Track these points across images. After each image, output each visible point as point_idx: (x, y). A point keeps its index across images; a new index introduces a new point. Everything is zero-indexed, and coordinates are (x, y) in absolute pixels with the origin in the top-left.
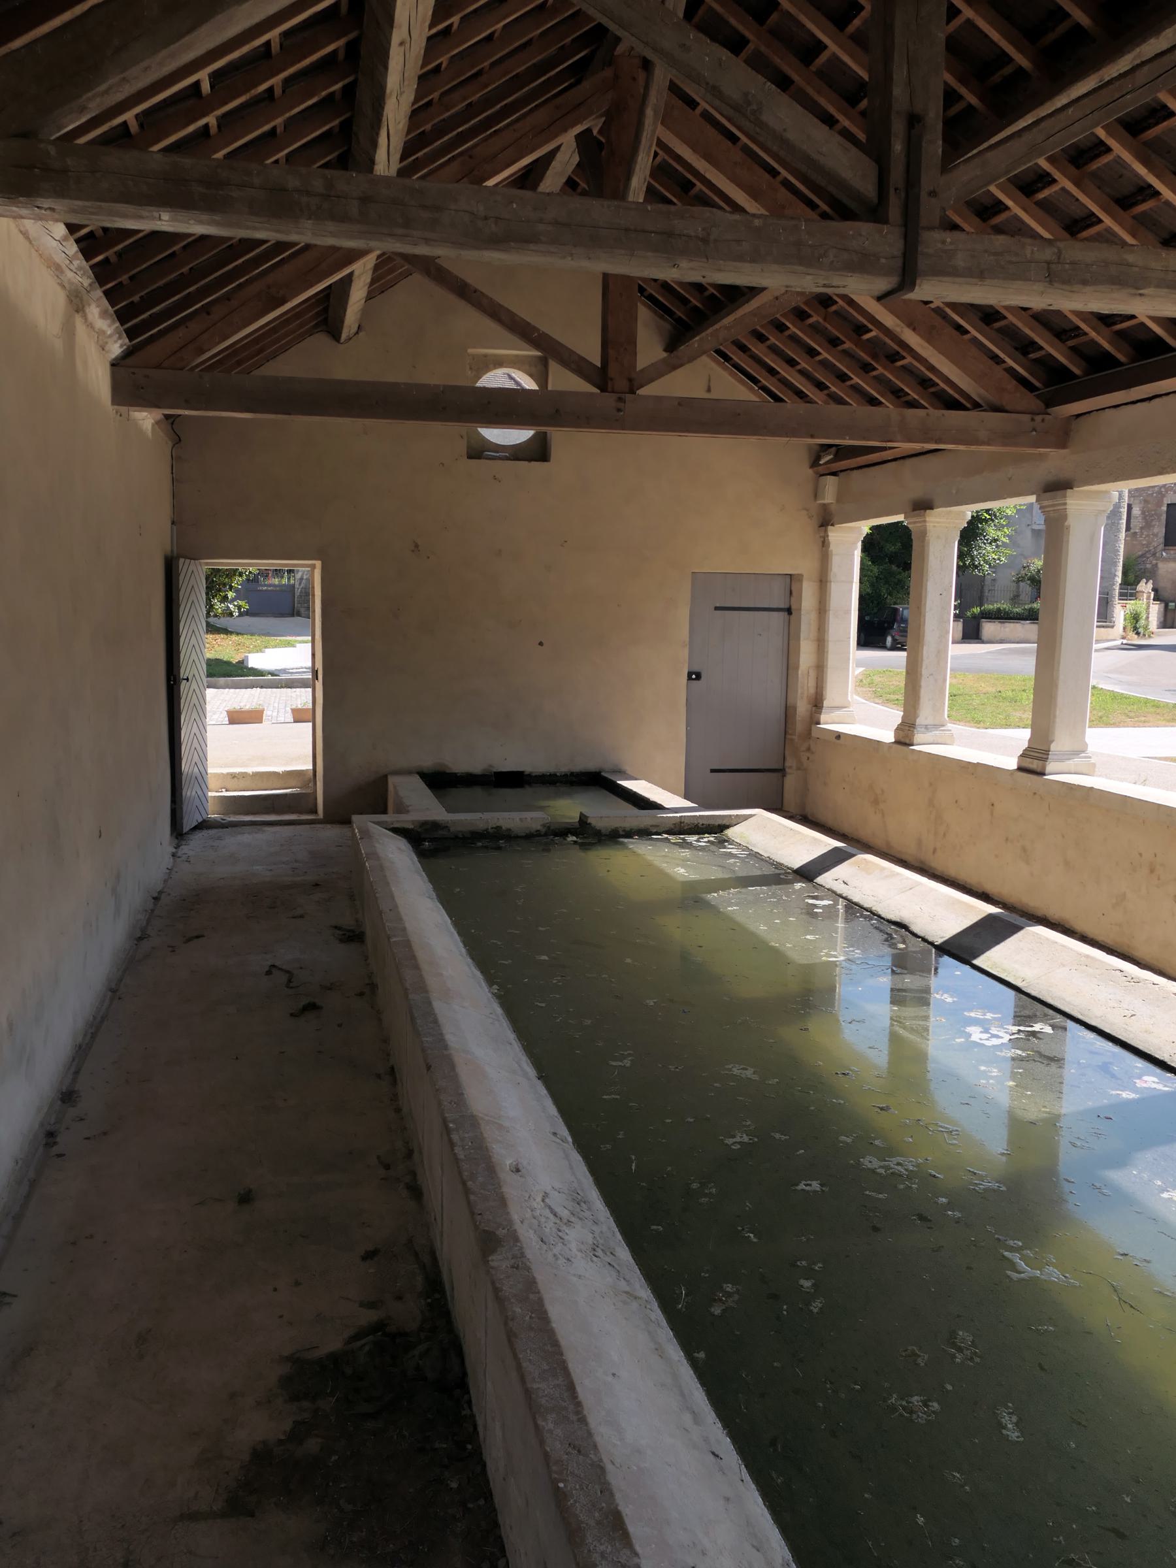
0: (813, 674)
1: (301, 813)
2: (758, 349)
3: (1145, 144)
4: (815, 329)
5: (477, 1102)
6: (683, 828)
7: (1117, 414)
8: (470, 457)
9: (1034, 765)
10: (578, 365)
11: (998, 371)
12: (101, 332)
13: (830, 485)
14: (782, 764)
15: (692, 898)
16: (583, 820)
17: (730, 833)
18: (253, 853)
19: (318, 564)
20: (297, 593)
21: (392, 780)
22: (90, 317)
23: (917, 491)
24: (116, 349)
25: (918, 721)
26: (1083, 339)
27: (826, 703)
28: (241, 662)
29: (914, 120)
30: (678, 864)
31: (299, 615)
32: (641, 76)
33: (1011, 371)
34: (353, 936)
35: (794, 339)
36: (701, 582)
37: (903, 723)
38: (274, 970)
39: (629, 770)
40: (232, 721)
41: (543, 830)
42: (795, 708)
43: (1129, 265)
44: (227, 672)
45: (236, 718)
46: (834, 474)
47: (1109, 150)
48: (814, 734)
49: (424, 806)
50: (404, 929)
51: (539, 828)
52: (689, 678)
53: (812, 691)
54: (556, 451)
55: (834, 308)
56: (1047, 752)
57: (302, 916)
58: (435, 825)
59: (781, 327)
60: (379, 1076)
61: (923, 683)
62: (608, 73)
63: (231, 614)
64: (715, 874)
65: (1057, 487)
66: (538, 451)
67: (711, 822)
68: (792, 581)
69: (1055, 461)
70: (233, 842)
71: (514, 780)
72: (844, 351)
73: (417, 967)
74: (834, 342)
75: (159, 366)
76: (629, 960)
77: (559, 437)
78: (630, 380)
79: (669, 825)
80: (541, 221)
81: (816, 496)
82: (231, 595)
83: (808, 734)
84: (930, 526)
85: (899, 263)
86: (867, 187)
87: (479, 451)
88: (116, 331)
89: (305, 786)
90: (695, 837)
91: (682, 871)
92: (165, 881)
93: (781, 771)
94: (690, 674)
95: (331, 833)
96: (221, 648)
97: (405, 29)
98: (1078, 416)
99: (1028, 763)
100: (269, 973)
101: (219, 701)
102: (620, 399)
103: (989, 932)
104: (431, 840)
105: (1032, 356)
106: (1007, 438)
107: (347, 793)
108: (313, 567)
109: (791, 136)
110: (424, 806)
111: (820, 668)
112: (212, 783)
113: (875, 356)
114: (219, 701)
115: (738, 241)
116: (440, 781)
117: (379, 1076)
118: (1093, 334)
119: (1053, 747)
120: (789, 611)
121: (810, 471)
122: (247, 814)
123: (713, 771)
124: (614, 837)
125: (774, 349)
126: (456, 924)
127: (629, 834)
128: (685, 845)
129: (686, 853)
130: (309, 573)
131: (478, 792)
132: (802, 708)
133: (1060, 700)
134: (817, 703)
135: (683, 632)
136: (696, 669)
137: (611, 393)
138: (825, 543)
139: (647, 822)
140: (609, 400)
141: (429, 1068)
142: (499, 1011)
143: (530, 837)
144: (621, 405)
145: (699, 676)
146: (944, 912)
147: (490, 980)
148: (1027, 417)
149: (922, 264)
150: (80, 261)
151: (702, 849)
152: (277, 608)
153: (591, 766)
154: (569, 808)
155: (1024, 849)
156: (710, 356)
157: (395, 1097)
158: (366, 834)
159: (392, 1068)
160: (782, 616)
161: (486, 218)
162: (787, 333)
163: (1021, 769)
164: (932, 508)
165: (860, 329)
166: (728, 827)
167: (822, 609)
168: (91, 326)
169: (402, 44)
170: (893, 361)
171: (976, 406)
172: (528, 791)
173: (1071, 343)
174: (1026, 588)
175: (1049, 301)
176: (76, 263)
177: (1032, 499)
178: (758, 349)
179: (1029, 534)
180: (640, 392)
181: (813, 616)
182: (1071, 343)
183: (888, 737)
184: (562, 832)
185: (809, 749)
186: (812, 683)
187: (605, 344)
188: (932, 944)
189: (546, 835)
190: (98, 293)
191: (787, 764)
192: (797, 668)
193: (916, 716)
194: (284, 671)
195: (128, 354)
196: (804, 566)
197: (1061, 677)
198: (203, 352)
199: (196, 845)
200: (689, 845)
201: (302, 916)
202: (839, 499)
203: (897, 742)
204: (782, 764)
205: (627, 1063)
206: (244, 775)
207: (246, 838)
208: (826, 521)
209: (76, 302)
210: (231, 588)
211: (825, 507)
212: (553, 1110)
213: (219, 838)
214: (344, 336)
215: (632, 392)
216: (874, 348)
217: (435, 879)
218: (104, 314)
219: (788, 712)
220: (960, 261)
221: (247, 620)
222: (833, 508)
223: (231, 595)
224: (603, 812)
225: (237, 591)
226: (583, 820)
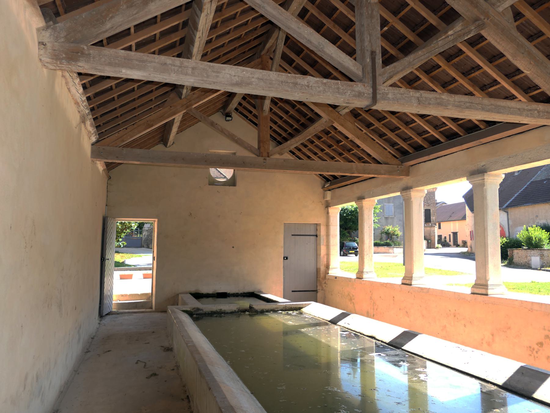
0: (325, 257)
1: (146, 309)
2: (304, 150)
3: (431, 77)
4: (324, 142)
5: (233, 402)
6: (287, 309)
7: (427, 165)
8: (209, 185)
9: (408, 282)
10: (249, 148)
11: (386, 152)
12: (89, 132)
13: (329, 194)
14: (316, 287)
15: (295, 331)
16: (251, 307)
17: (303, 310)
18: (129, 321)
19: (156, 220)
20: (143, 240)
21: (180, 296)
22: (87, 125)
23: (358, 193)
24: (94, 139)
25: (364, 270)
26: (412, 141)
27: (330, 267)
28: (123, 262)
29: (373, 53)
30: (290, 320)
31: (143, 247)
32: (270, 61)
33: (389, 152)
34: (169, 349)
35: (317, 146)
36: (287, 227)
37: (359, 271)
38: (139, 362)
39: (263, 290)
40: (121, 279)
41: (237, 310)
42: (320, 269)
43: (443, 99)
44: (120, 265)
45: (122, 277)
46: (329, 190)
47: (420, 79)
48: (327, 277)
49: (194, 304)
50: (192, 341)
51: (235, 309)
52: (284, 259)
53: (325, 263)
54: (238, 183)
55: (330, 135)
56: (412, 277)
57: (148, 343)
58: (198, 309)
59: (312, 142)
60: (183, 400)
61: (365, 257)
62: (259, 60)
63: (120, 246)
64: (303, 323)
65: (407, 189)
66: (232, 182)
67: (296, 306)
68: (317, 225)
69: (405, 180)
70: (121, 319)
71: (223, 295)
72: (333, 149)
73: (199, 353)
74: (330, 146)
75: (108, 145)
76: (276, 352)
77: (243, 173)
78: (268, 153)
79: (282, 308)
80: (253, 77)
81: (324, 198)
82: (120, 240)
83: (325, 278)
84: (364, 205)
85: (371, 96)
86: (360, 73)
87: (213, 182)
88: (95, 132)
89: (148, 299)
90: (292, 312)
91: (291, 323)
92: (96, 332)
93: (316, 291)
94: (284, 258)
95: (158, 316)
96: (118, 258)
97: (201, 32)
98: (412, 166)
99: (405, 282)
100: (137, 363)
101: (117, 274)
102: (265, 159)
103: (408, 336)
104: (197, 314)
105: (395, 147)
106: (390, 173)
107: (160, 305)
108: (155, 221)
109: (334, 56)
110: (194, 304)
111: (328, 255)
112: (114, 298)
113: (343, 150)
114: (117, 274)
115: (319, 87)
116: (198, 296)
117: (183, 400)
118: (416, 139)
119: (414, 275)
120: (317, 236)
121: (322, 190)
122: (126, 309)
123: (293, 291)
124: (262, 312)
125: (310, 150)
126: (210, 341)
127: (268, 311)
128: (288, 314)
129: (288, 317)
130: (153, 224)
131: (210, 299)
132: (323, 268)
133: (414, 259)
134: (327, 267)
135: (282, 244)
136: (286, 256)
137: (260, 159)
138: (328, 213)
139: (274, 308)
140: (260, 159)
141: (210, 389)
142: (232, 370)
143: (232, 313)
144: (265, 161)
145: (287, 258)
146: (388, 332)
147: (226, 360)
148: (396, 166)
149: (378, 96)
150: (86, 103)
151: (295, 316)
152: (138, 243)
153: (251, 290)
154: (245, 303)
155: (407, 312)
156: (288, 153)
157: (190, 407)
158: (173, 312)
159: (188, 396)
160: (314, 237)
161: (235, 76)
162: (314, 144)
163: (403, 284)
164: (364, 199)
165: (339, 142)
166: (302, 308)
167: (328, 235)
168: (86, 128)
169: (199, 38)
170: (349, 152)
171: (379, 163)
172: (228, 299)
173: (408, 143)
174: (384, 236)
175: (418, 110)
176: (85, 103)
177: (398, 194)
178: (304, 150)
179: (384, 218)
180: (272, 157)
181: (325, 237)
182: (408, 143)
183: (353, 276)
184: (244, 311)
185: (325, 283)
186: (325, 260)
187: (259, 142)
188: (385, 343)
189: (238, 312)
190: (90, 117)
191: (318, 288)
192: (320, 255)
193: (363, 269)
194: (138, 265)
195: (97, 142)
196: (321, 220)
197: (414, 251)
198: (123, 141)
199: (108, 319)
200: (290, 315)
201: (148, 343)
202: (332, 199)
203: (357, 278)
204: (316, 287)
205: (284, 388)
206: (126, 295)
207: (126, 317)
208: (328, 206)
209: (83, 121)
210: (121, 238)
211: (327, 201)
212: (260, 405)
213: (116, 318)
214: (168, 145)
215: (268, 157)
216: (344, 147)
217: (199, 326)
218: (91, 125)
219: (318, 270)
220: (390, 96)
221: (125, 249)
222: (330, 201)
223: (120, 240)
224: (258, 305)
225: (123, 238)
226: (251, 307)
